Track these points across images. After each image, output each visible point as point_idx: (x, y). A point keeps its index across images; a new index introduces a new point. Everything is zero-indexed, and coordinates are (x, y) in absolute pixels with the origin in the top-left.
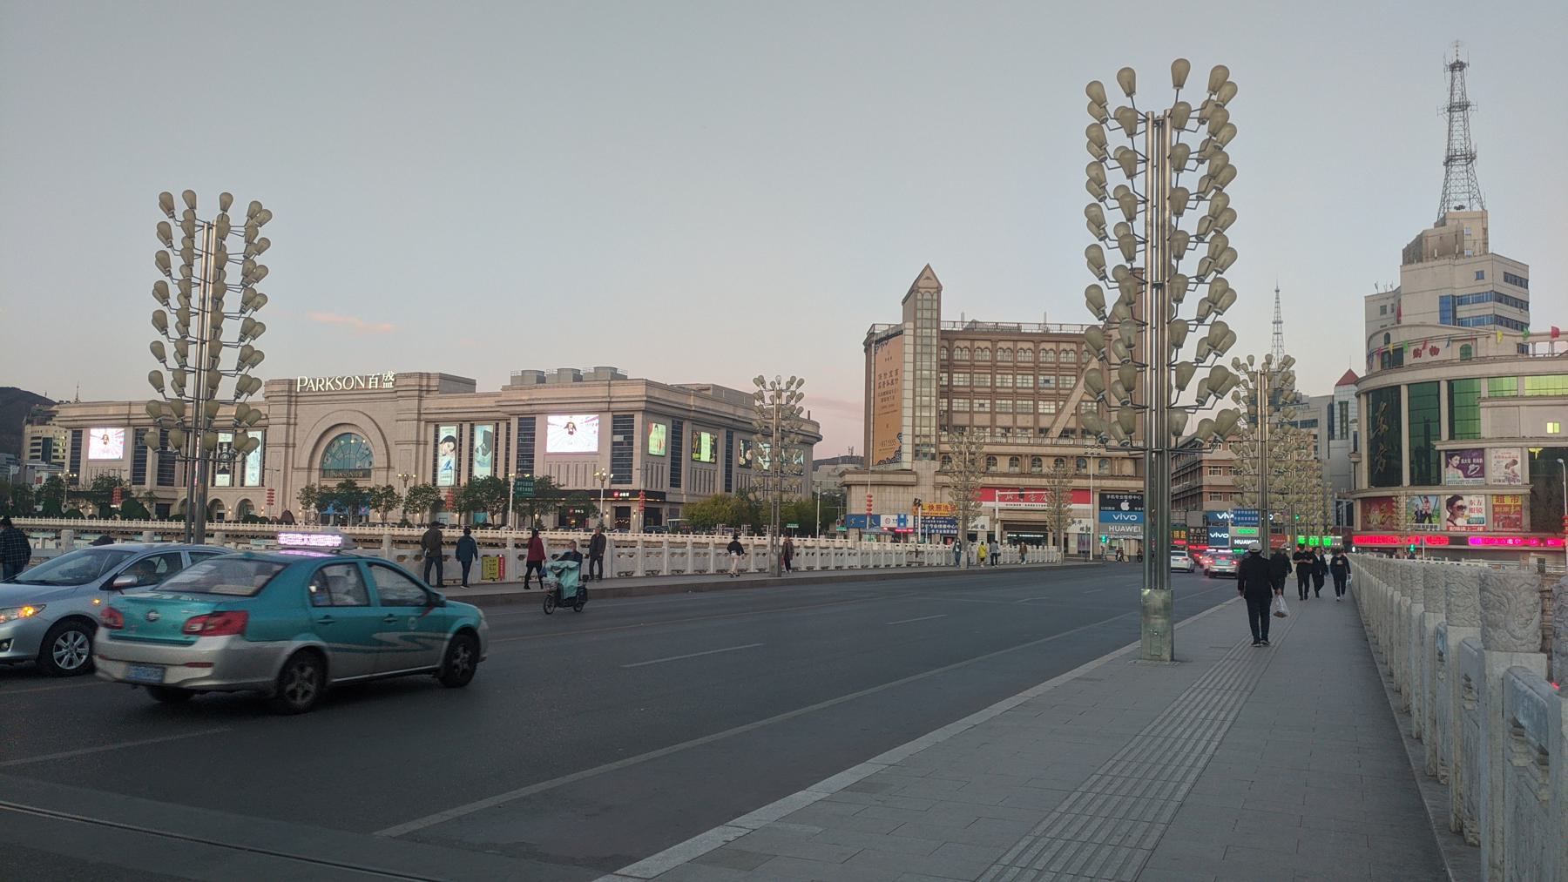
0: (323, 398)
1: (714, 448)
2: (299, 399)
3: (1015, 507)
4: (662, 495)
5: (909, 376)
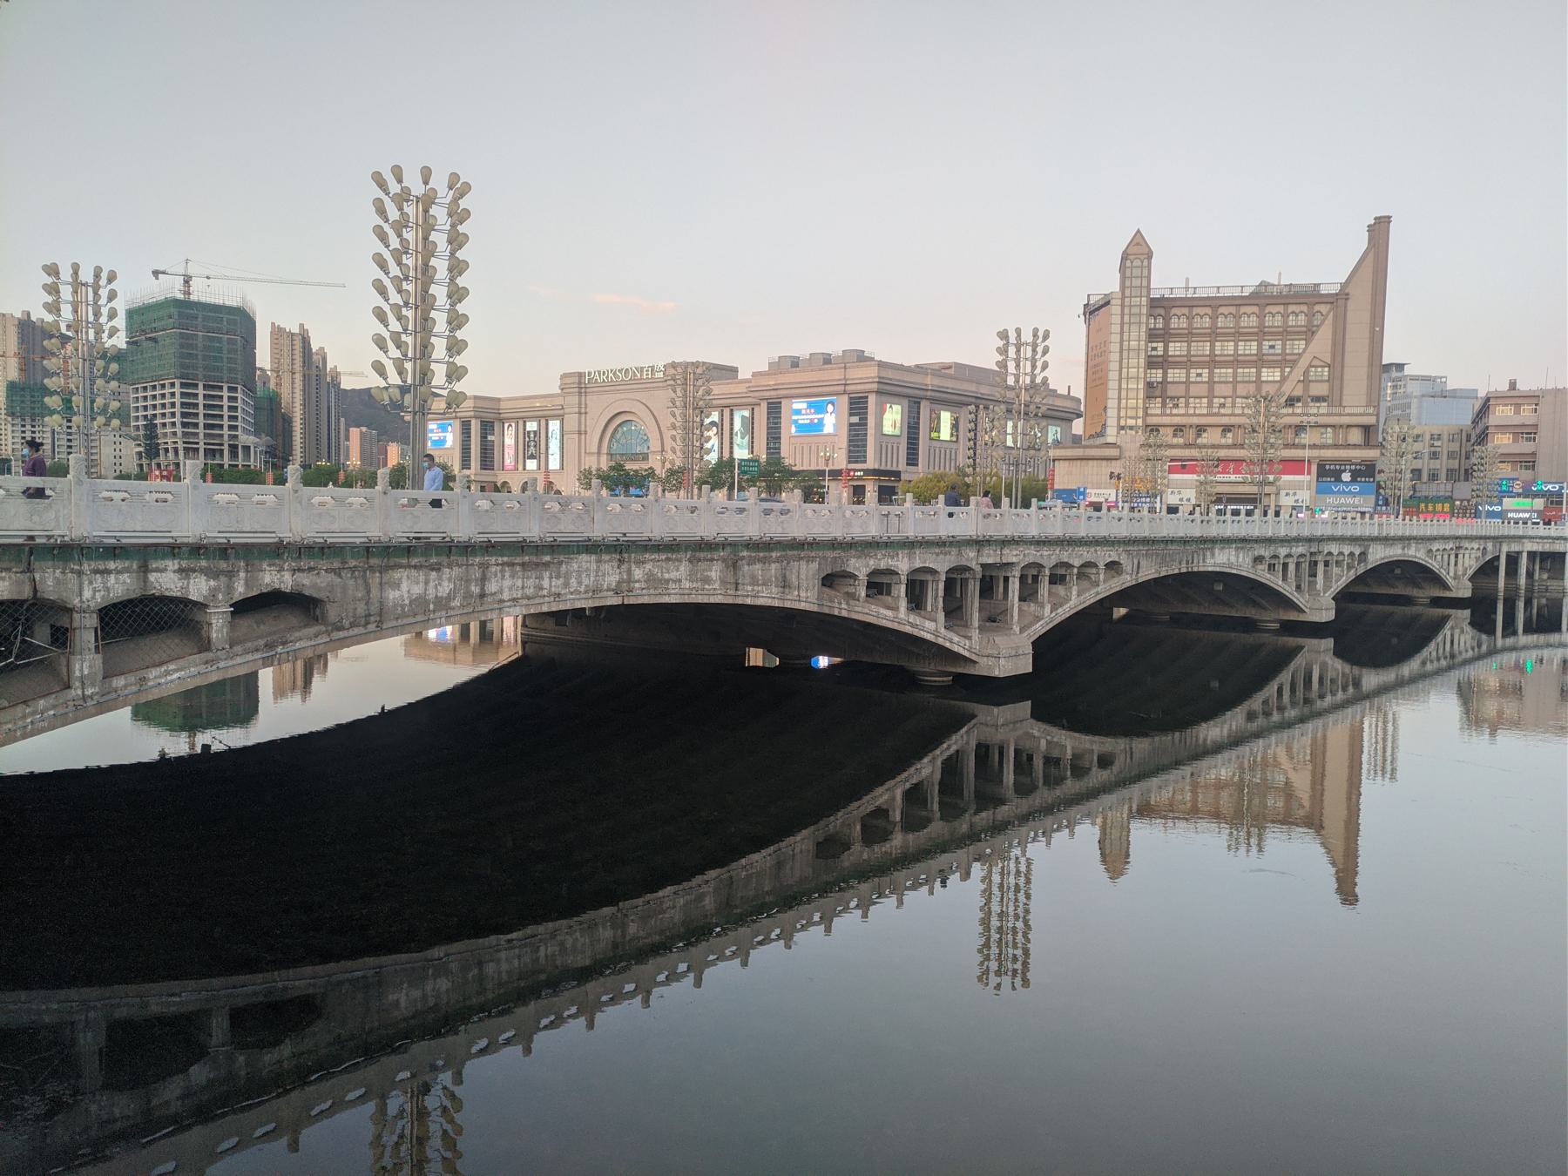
0: (607, 389)
1: (955, 426)
2: (588, 390)
3: (1225, 480)
4: (897, 474)
5: (1115, 347)
